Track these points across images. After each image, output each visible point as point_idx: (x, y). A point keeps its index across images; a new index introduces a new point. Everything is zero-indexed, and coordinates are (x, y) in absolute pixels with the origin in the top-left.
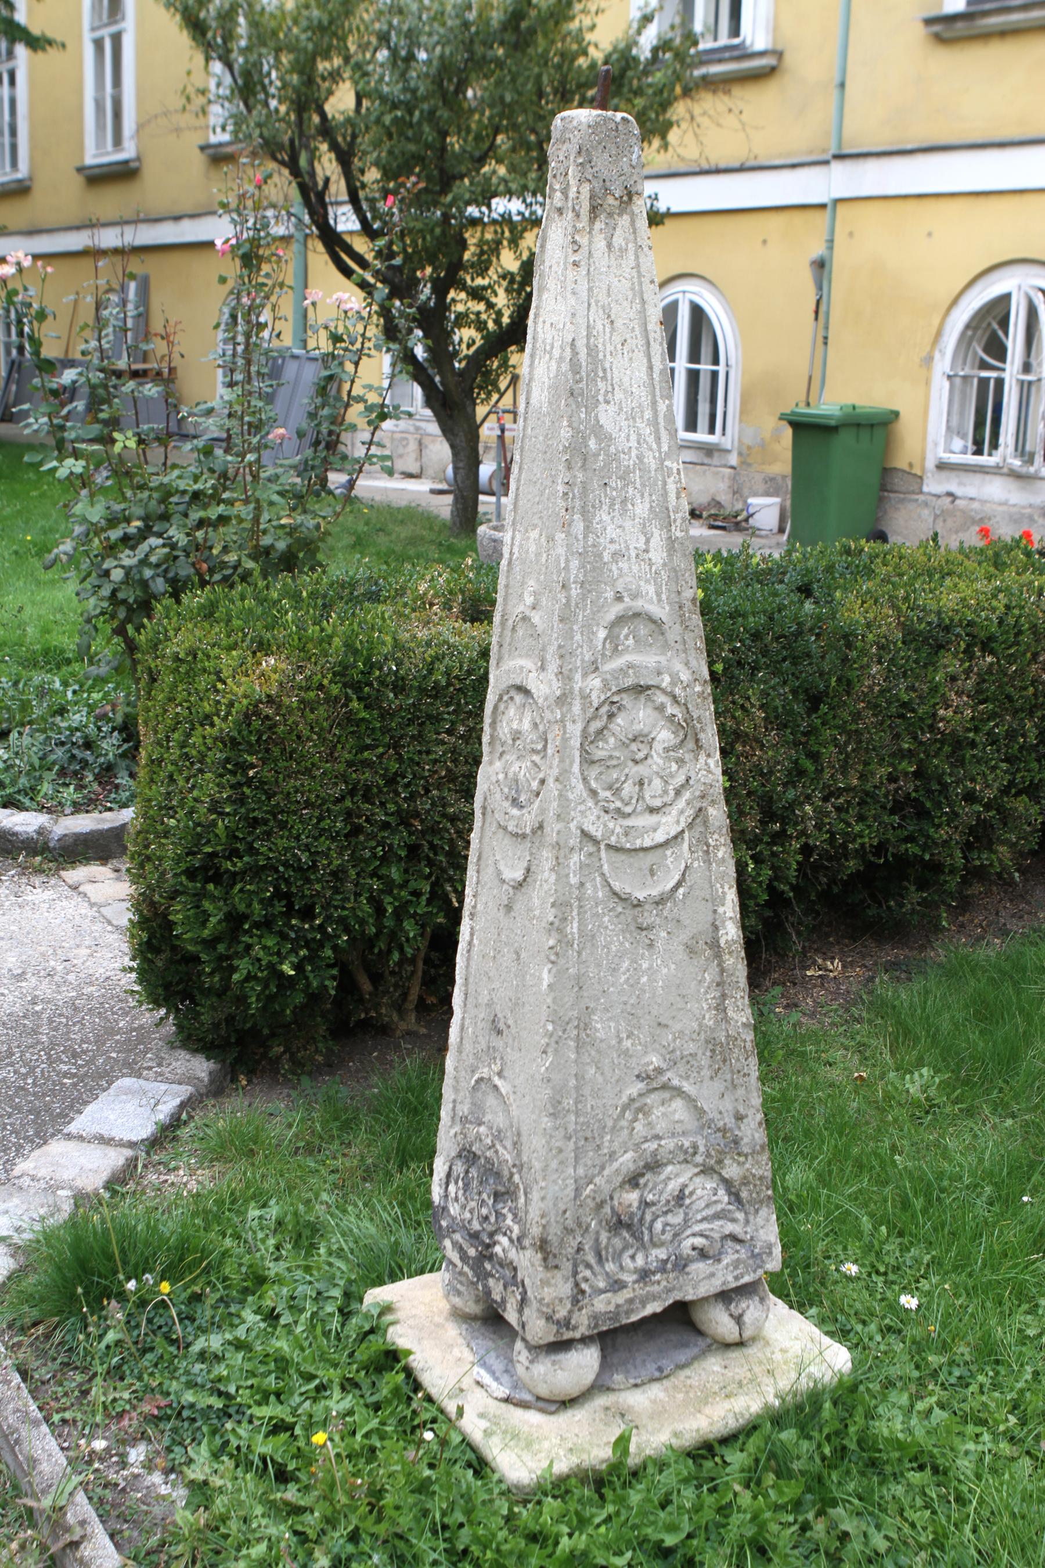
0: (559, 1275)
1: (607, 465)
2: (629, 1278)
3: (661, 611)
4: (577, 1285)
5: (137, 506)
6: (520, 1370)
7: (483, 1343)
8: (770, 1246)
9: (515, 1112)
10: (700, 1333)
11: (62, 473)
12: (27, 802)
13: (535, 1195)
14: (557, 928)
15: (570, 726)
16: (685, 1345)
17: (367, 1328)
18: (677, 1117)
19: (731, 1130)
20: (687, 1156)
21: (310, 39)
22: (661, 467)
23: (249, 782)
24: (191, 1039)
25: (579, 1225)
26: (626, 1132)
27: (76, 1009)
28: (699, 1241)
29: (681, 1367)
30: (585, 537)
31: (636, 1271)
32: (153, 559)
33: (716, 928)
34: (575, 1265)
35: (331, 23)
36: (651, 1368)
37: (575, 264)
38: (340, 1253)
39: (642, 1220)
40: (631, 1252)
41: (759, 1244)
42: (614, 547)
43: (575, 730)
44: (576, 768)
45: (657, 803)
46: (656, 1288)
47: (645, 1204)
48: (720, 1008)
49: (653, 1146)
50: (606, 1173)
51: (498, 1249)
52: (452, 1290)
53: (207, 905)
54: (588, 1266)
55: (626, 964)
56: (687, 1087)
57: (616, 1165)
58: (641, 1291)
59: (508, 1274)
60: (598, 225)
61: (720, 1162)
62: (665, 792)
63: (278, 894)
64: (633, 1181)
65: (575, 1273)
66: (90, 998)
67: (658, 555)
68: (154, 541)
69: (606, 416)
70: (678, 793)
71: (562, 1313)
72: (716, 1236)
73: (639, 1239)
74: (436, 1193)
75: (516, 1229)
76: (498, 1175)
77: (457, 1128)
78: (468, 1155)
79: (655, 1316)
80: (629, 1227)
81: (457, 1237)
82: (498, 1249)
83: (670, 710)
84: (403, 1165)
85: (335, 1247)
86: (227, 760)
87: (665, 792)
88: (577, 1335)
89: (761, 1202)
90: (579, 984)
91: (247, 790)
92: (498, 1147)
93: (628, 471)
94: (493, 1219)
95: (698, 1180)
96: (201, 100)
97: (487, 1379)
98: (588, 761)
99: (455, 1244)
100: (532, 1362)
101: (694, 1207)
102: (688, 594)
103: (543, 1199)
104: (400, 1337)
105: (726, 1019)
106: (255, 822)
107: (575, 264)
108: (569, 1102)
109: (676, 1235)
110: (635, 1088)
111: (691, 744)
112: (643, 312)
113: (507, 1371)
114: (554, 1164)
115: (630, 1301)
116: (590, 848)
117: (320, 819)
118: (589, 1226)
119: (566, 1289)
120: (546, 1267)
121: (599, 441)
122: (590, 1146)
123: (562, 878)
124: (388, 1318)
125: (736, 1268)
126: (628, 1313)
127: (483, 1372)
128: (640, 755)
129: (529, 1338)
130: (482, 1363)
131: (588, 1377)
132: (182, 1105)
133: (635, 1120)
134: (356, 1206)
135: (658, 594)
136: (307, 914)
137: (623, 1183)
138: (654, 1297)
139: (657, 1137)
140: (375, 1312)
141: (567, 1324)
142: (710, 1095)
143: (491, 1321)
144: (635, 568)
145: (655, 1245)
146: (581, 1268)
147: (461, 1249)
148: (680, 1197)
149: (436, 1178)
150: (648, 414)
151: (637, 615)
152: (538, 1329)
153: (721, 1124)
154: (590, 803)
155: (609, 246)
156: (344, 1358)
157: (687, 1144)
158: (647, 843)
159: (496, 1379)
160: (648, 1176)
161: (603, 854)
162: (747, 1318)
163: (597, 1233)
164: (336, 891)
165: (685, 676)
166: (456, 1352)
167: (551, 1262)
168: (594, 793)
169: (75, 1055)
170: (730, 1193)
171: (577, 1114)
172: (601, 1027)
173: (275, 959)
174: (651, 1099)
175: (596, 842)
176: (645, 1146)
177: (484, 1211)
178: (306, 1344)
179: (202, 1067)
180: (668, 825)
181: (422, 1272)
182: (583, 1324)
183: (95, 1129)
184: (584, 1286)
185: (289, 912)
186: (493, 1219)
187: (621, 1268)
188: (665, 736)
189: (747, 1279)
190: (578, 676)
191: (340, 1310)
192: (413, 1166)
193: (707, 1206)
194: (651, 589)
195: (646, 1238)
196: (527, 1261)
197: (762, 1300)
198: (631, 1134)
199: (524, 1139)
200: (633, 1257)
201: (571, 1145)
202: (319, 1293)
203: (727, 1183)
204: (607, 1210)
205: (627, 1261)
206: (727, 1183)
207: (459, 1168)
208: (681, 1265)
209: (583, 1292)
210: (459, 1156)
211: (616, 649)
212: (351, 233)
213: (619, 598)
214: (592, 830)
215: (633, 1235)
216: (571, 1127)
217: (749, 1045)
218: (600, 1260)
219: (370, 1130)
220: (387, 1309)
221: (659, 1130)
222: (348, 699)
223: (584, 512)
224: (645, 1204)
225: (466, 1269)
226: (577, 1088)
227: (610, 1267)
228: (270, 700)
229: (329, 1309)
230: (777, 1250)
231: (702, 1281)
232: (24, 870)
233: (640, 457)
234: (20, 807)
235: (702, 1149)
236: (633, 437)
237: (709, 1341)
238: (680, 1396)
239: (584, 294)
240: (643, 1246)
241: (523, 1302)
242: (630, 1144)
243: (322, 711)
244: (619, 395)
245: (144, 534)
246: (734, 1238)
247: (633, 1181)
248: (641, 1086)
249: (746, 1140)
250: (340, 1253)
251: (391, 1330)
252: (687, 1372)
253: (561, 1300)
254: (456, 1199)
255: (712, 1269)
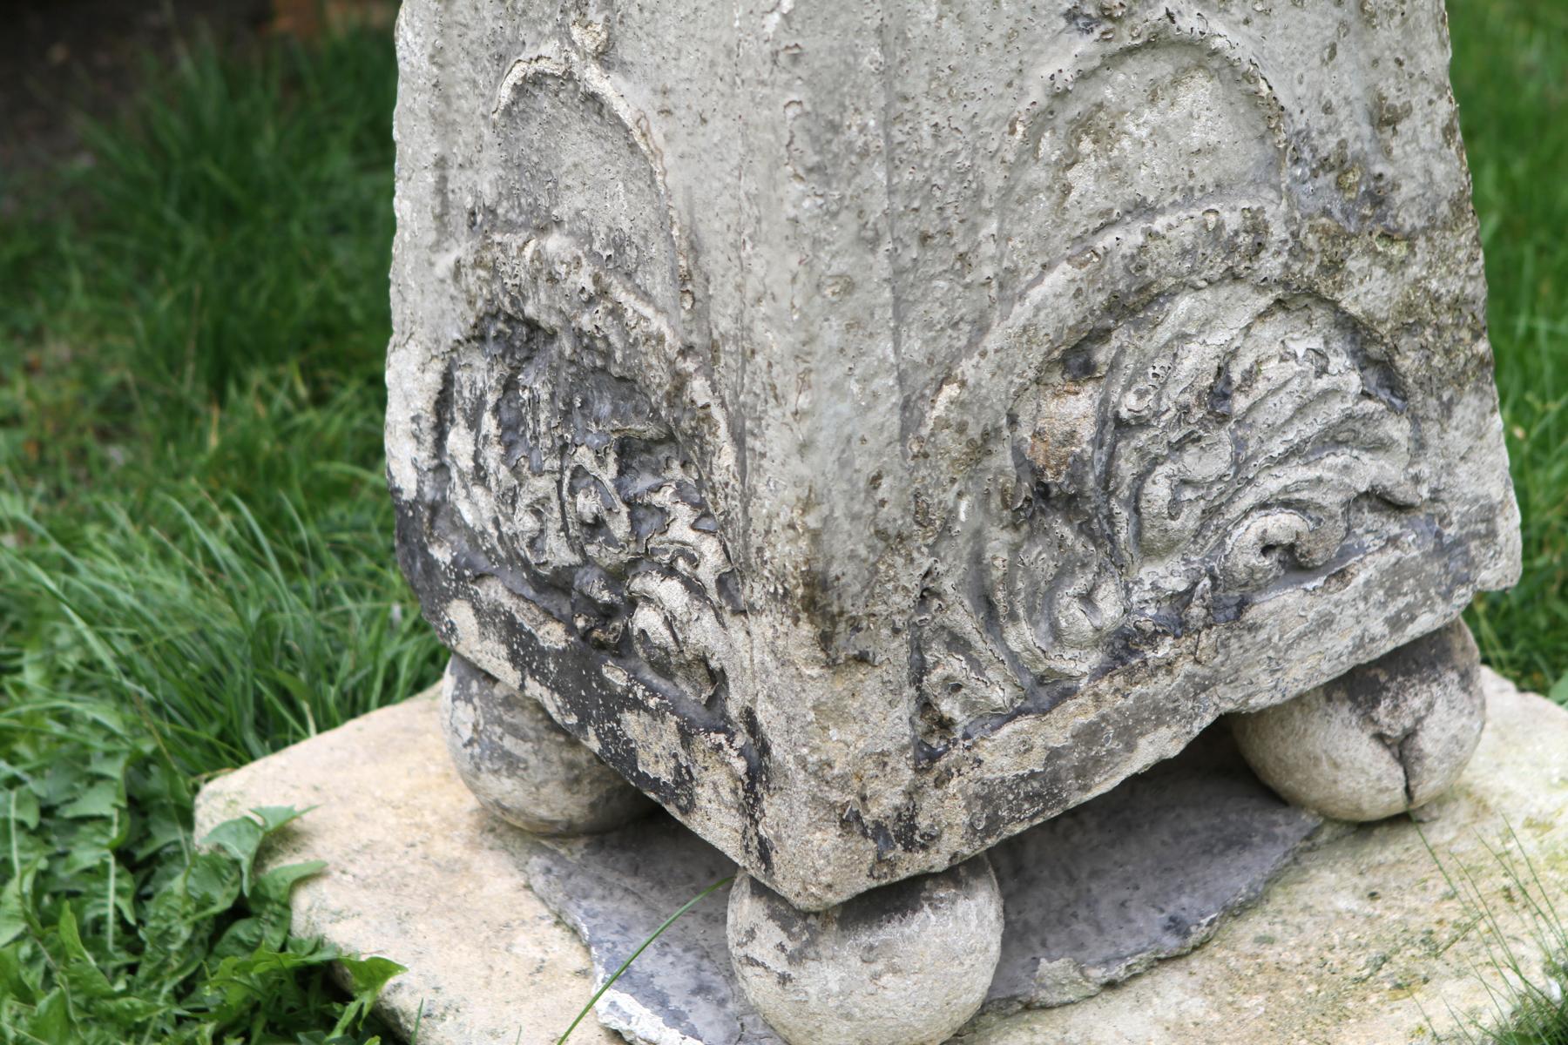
0: (869, 680)
2: (1079, 664)
4: (926, 705)
6: (758, 987)
7: (612, 908)
8: (1489, 514)
9: (674, 175)
10: (1277, 798)
13: (775, 440)
16: (1238, 842)
17: (223, 903)
18: (1196, 138)
19: (1361, 160)
20: (1233, 257)
26: (1044, 202)
28: (1281, 524)
29: (1238, 911)
31: (1101, 638)
34: (918, 647)
36: (1149, 924)
38: (87, 678)
39: (1108, 475)
40: (1081, 583)
41: (1456, 511)
46: (1162, 685)
47: (1118, 426)
49: (1130, 237)
50: (992, 341)
51: (646, 619)
52: (485, 755)
54: (957, 643)
56: (1224, 34)
58: (1117, 698)
59: (690, 692)
61: (1333, 266)
64: (1076, 360)
65: (920, 670)
71: (887, 800)
72: (1331, 500)
73: (1099, 534)
74: (404, 462)
75: (711, 554)
76: (628, 385)
77: (461, 249)
78: (510, 333)
79: (1162, 770)
80: (1070, 504)
81: (494, 592)
82: (646, 619)
84: (220, 381)
85: (71, 660)
88: (938, 860)
89: (1459, 379)
92: (620, 294)
94: (620, 527)
95: (1266, 331)
99: (486, 615)
100: (796, 958)
101: (1261, 417)
103: (804, 448)
104: (339, 917)
108: (862, 125)
109: (1211, 513)
110: (1068, 54)
113: (702, 989)
114: (831, 334)
115: (1089, 735)
118: (952, 513)
119: (893, 723)
120: (831, 664)
122: (939, 260)
124: (287, 864)
125: (1393, 592)
126: (1083, 772)
127: (626, 1001)
129: (787, 888)
130: (621, 975)
131: (976, 982)
133: (1071, 160)
134: (109, 523)
137: (1048, 365)
138: (1158, 714)
139: (1142, 208)
140: (242, 850)
141: (905, 831)
143: (630, 832)
145: (1148, 552)
146: (936, 651)
147: (512, 632)
148: (1218, 394)
149: (398, 415)
152: (818, 860)
153: (1329, 145)
156: (163, 1006)
157: (1233, 221)
159: (675, 1018)
160: (1120, 337)
162: (1429, 742)
163: (978, 535)
166: (526, 946)
167: (846, 643)
170: (1364, 362)
171: (893, 165)
176: (1106, 240)
177: (587, 505)
178: (33, 977)
181: (354, 706)
182: (952, 822)
184: (948, 707)
186: (620, 527)
187: (1056, 634)
189: (1425, 622)
191: (123, 855)
192: (257, 377)
193: (1301, 410)
195: (1124, 534)
196: (760, 654)
197: (1466, 678)
198: (1060, 208)
199: (715, 260)
200: (1087, 598)
201: (881, 264)
202: (47, 811)
203: (1356, 330)
204: (1003, 458)
205: (1072, 614)
206: (1356, 330)
207: (480, 374)
208: (1231, 602)
209: (945, 725)
210: (478, 337)
215: (1085, 530)
216: (878, 205)
218: (991, 614)
219: (98, 287)
220: (278, 837)
221: (1143, 185)
224: (1118, 426)
225: (535, 689)
226: (886, 74)
227: (1022, 636)
229: (87, 855)
230: (1510, 525)
235: (1278, 232)
237: (1307, 820)
238: (1255, 1003)
240: (1119, 564)
241: (758, 776)
242: (1058, 241)
246: (1382, 501)
247: (1076, 360)
248: (1085, 45)
249: (1407, 189)
250: (87, 678)
251: (303, 900)
252: (1257, 924)
253: (882, 759)
254: (480, 475)
255: (1322, 605)
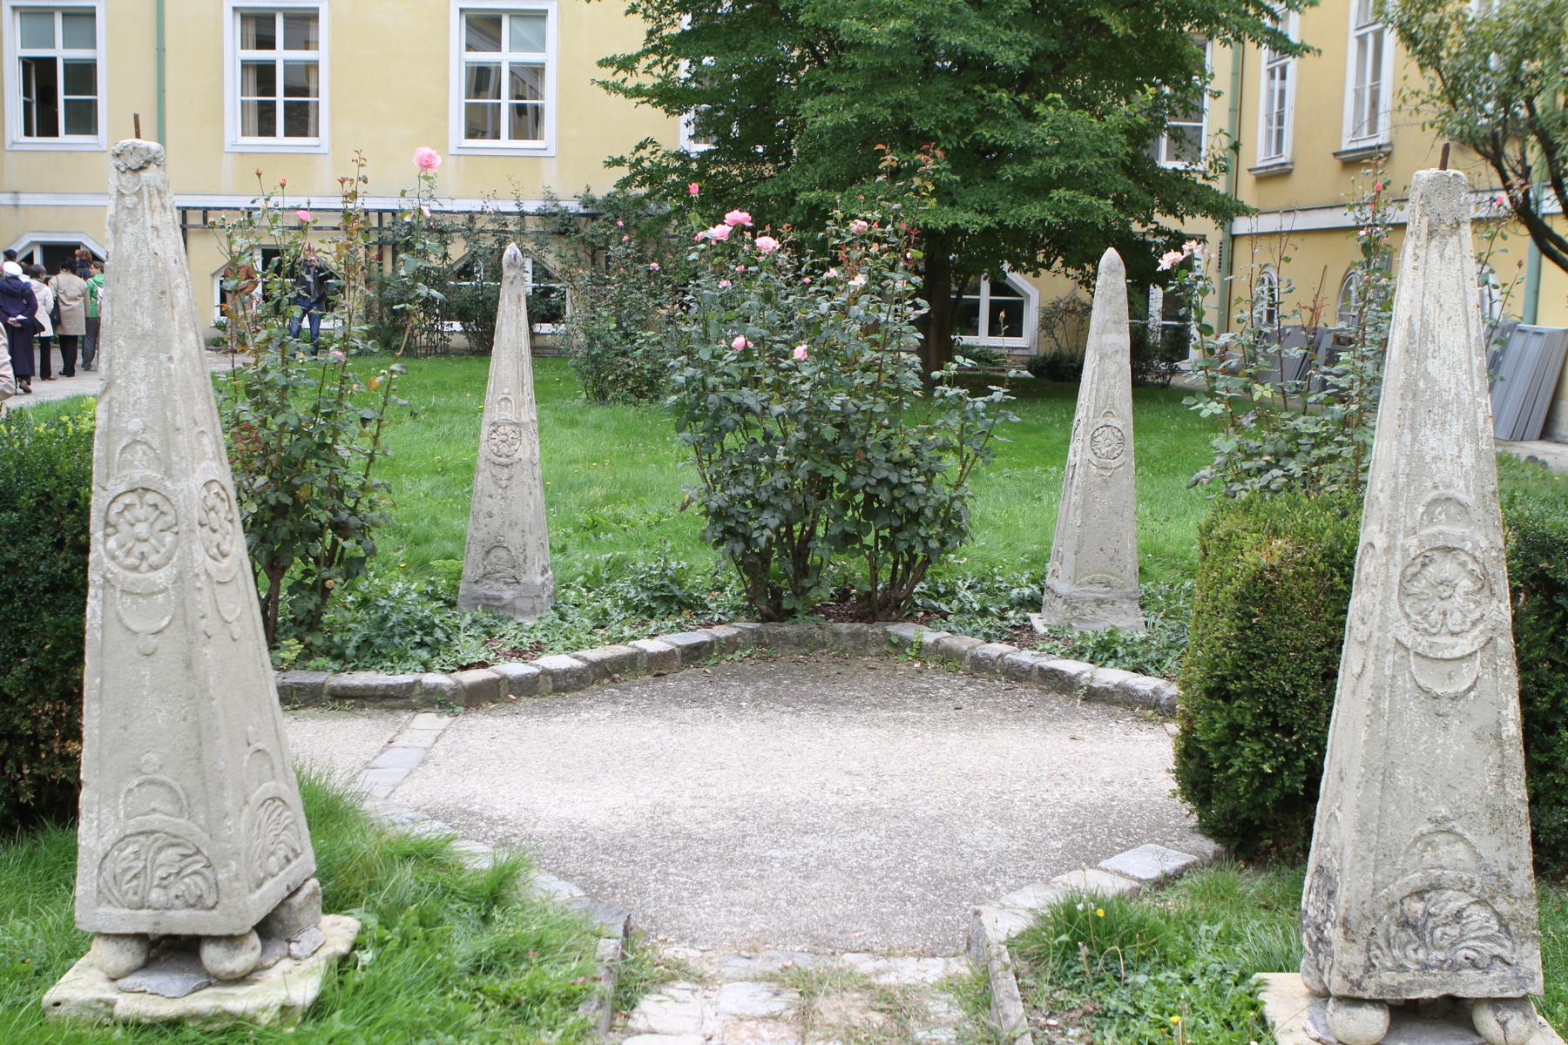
0: (1355, 947)
1: (1432, 398)
3: (1469, 499)
5: (1269, 441)
8: (1533, 974)
11: (1205, 414)
12: (1152, 670)
14: (1374, 702)
15: (1392, 568)
21: (1515, 45)
22: (1473, 401)
23: (1251, 627)
24: (1209, 829)
25: (1374, 915)
26: (1416, 858)
27: (1141, 808)
28: (1471, 954)
30: (1412, 445)
32: (1273, 487)
33: (1500, 725)
34: (1369, 944)
35: (1535, 29)
37: (1415, 268)
42: (1434, 453)
43: (1396, 572)
44: (1395, 597)
45: (1457, 629)
48: (1500, 783)
53: (1215, 714)
54: (1379, 947)
55: (1425, 738)
56: (1468, 835)
57: (1406, 879)
58: (1420, 978)
60: (1434, 243)
61: (1493, 898)
62: (1464, 622)
63: (1266, 713)
64: (1419, 894)
65: (1368, 950)
66: (1154, 803)
67: (1468, 460)
68: (1276, 472)
69: (1433, 367)
70: (1474, 624)
71: (1355, 976)
73: (1422, 938)
78: (1320, 870)
80: (1414, 927)
83: (1470, 566)
86: (1239, 610)
87: (1464, 622)
90: (1387, 744)
91: (1249, 632)
93: (1447, 403)
95: (1475, 908)
96: (1416, 101)
97: (1310, 1026)
98: (1404, 593)
102: (1491, 488)
105: (1504, 793)
106: (1254, 657)
107: (1415, 268)
108: (1373, 825)
110: (1426, 827)
111: (1487, 593)
112: (1465, 298)
114: (1358, 867)
115: (1411, 982)
116: (1402, 652)
117: (1303, 660)
119: (1361, 959)
121: (1427, 382)
123: (1379, 669)
128: (1446, 595)
132: (1186, 867)
135: (1467, 487)
136: (1288, 732)
138: (1431, 986)
139: (1442, 867)
141: (1358, 985)
142: (1488, 847)
144: (1450, 468)
146: (1373, 947)
148: (1458, 915)
150: (1465, 366)
151: (1448, 499)
154: (1404, 622)
155: (1441, 256)
158: (1447, 655)
160: (1432, 893)
161: (1412, 658)
164: (1312, 717)
165: (1484, 544)
167: (1350, 936)
168: (1408, 616)
169: (1129, 834)
172: (1402, 778)
173: (1259, 759)
174: (1438, 838)
175: (1407, 649)
179: (1209, 846)
180: (1464, 646)
183: (1118, 867)
185: (1274, 727)
188: (1465, 584)
190: (1400, 536)
194: (1462, 483)
201: (1372, 856)
204: (1397, 910)
209: (1374, 966)
211: (1431, 521)
212: (1552, 215)
213: (1436, 487)
214: (1404, 640)
217: (1523, 816)
222: (1333, 575)
223: (1412, 428)
227: (1396, 952)
228: (1273, 569)
230: (1540, 979)
231: (1470, 985)
232: (1137, 718)
233: (1458, 395)
234: (1145, 672)
235: (1478, 884)
236: (1453, 381)
239: (1420, 288)
243: (1311, 582)
244: (1443, 353)
245: (1269, 467)
247: (1419, 894)
